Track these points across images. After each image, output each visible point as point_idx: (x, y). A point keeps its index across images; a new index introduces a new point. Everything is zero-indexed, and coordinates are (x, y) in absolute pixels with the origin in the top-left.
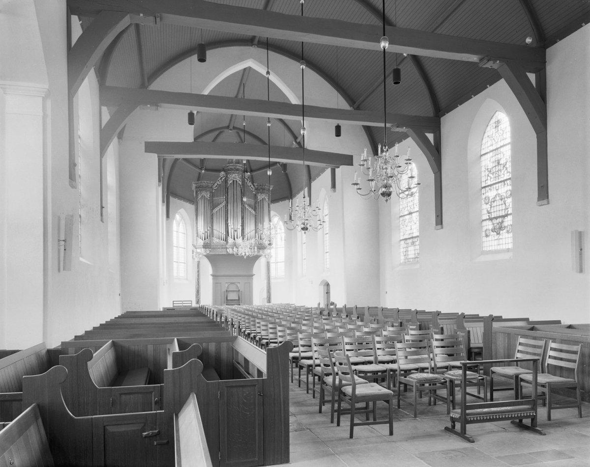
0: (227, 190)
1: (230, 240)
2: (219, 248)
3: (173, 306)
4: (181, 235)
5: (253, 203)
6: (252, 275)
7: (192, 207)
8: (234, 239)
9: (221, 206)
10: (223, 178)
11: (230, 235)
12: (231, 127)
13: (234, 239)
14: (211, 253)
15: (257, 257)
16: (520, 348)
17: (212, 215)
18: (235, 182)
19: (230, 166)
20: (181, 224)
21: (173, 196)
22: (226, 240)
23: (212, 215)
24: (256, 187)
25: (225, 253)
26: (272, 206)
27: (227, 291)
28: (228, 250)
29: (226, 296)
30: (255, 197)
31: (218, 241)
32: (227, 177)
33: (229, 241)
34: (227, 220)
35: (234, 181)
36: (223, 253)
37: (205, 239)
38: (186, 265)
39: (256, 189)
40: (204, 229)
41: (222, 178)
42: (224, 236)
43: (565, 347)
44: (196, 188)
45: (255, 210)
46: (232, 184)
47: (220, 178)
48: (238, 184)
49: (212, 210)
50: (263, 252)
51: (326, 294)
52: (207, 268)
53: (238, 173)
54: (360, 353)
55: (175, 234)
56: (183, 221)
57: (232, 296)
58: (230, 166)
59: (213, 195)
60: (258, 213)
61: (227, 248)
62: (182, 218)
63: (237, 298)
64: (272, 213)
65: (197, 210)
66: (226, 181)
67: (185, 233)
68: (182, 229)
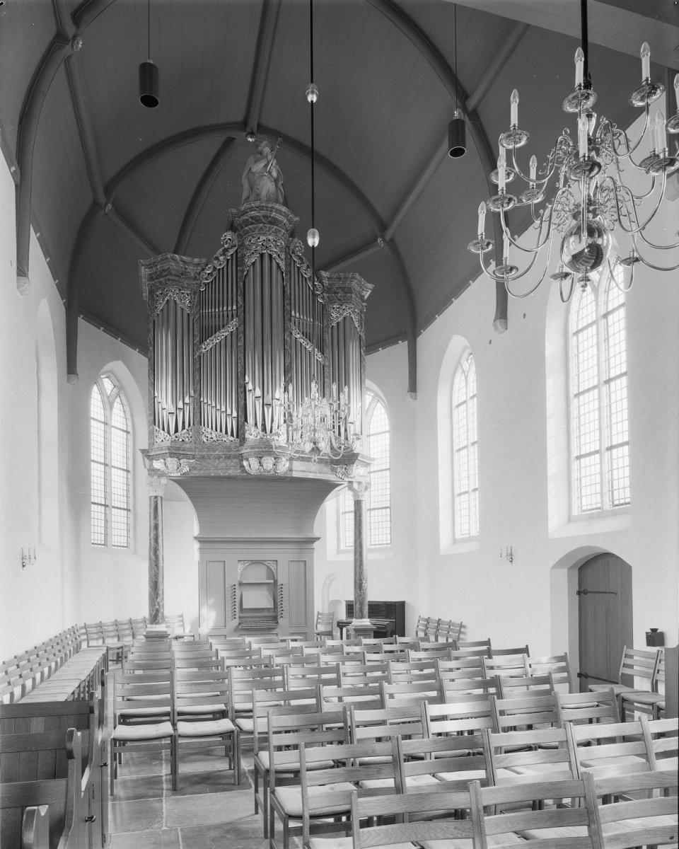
1: (252, 434)
2: (219, 457)
6: (313, 540)
7: (141, 361)
8: (264, 429)
9: (224, 333)
10: (231, 252)
11: (251, 420)
12: (253, 124)
13: (264, 429)
14: (196, 473)
15: (325, 488)
17: (198, 362)
18: (266, 259)
19: (252, 209)
20: (117, 405)
21: (86, 319)
22: (240, 434)
23: (198, 362)
24: (326, 282)
25: (237, 472)
26: (369, 359)
28: (245, 463)
29: (238, 600)
30: (323, 313)
32: (242, 245)
33: (247, 435)
34: (242, 392)
35: (262, 255)
36: (231, 472)
37: (176, 431)
40: (175, 402)
41: (226, 250)
42: (232, 424)
44: (151, 278)
46: (258, 265)
47: (221, 250)
49: (196, 347)
50: (346, 474)
51: (577, 597)
52: (185, 523)
53: (276, 232)
54: (219, 703)
55: (96, 430)
56: (123, 398)
57: (258, 599)
58: (252, 209)
59: (201, 301)
60: (334, 376)
61: (241, 458)
62: (120, 388)
64: (368, 383)
65: (152, 370)
66: (238, 260)
67: (130, 429)
68: (118, 417)
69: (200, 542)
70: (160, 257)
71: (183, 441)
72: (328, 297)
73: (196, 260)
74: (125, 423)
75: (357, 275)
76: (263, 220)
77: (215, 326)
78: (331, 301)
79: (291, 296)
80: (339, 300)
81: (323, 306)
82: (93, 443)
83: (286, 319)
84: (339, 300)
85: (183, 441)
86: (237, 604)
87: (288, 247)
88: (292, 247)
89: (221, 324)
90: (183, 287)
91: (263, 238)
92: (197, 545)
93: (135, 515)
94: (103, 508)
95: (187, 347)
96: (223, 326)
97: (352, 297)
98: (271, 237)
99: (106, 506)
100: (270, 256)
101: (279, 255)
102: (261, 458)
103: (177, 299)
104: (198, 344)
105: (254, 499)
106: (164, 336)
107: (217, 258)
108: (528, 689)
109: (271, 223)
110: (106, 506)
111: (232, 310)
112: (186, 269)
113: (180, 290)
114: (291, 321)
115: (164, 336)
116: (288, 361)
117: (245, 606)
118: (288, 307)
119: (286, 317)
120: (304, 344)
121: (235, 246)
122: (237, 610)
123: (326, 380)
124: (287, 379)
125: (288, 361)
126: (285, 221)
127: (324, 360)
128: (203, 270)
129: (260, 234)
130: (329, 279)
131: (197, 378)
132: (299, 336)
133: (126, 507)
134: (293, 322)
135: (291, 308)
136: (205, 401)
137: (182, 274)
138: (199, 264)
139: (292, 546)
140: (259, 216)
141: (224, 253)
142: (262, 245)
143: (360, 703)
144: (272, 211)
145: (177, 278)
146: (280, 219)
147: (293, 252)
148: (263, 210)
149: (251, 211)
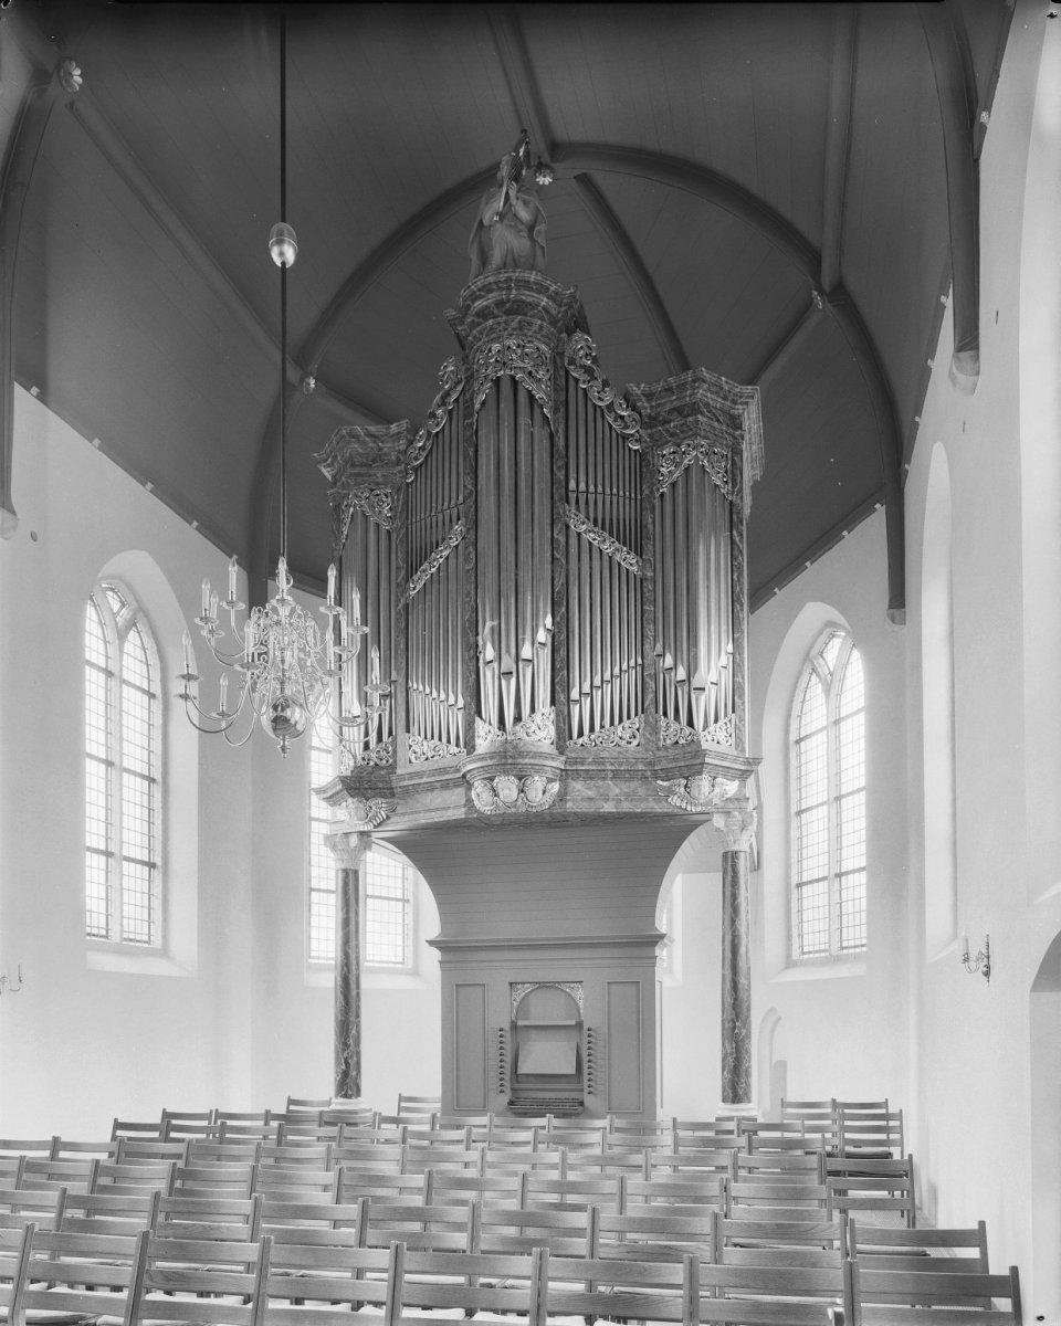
0: (471, 451)
3: (288, 1111)
4: (134, 703)
5: (626, 512)
6: (655, 940)
16: (131, 1262)
18: (506, 388)
25: (460, 814)
27: (514, 1027)
29: (508, 1059)
30: (643, 467)
31: (426, 747)
38: (409, 909)
39: (650, 422)
41: (447, 394)
43: (488, 580)
45: (639, 552)
47: (438, 397)
48: (523, 398)
57: (548, 1057)
63: (572, 1070)
69: (440, 949)
70: (689, 376)
71: (376, 765)
72: (651, 436)
73: (394, 428)
74: (146, 733)
75: (706, 374)
76: (496, 311)
77: (432, 543)
78: (657, 442)
79: (567, 451)
80: (672, 435)
81: (641, 455)
82: (862, 823)
83: (556, 497)
84: (672, 435)
85: (376, 765)
86: (508, 1066)
87: (558, 354)
88: (568, 352)
89: (440, 537)
90: (377, 484)
91: (496, 347)
92: (436, 954)
93: (165, 874)
94: (401, 904)
95: (387, 592)
96: (443, 539)
97: (697, 422)
98: (512, 343)
99: (108, 854)
100: (515, 383)
101: (530, 373)
102: (492, 779)
103: (366, 509)
104: (403, 583)
105: (566, 874)
106: (712, 550)
107: (433, 415)
108: (647, 1178)
109: (509, 312)
110: (108, 854)
111: (587, 492)
112: (380, 449)
113: (372, 490)
114: (568, 502)
115: (712, 550)
116: (559, 582)
117: (523, 1070)
118: (561, 475)
119: (560, 494)
120: (595, 543)
121: (459, 382)
122: (507, 1077)
123: (646, 607)
124: (558, 619)
125: (559, 582)
126: (544, 301)
127: (642, 568)
128: (411, 443)
129: (492, 341)
130: (649, 396)
131: (402, 646)
132: (584, 527)
133: (103, 847)
134: (573, 501)
135: (567, 476)
136: (415, 686)
137: (374, 461)
138: (399, 433)
139: (608, 953)
140: (487, 307)
141: (443, 403)
142: (497, 361)
143: (239, 1119)
144: (509, 288)
145: (363, 470)
146: (530, 299)
147: (572, 362)
148: (491, 291)
149: (474, 301)
